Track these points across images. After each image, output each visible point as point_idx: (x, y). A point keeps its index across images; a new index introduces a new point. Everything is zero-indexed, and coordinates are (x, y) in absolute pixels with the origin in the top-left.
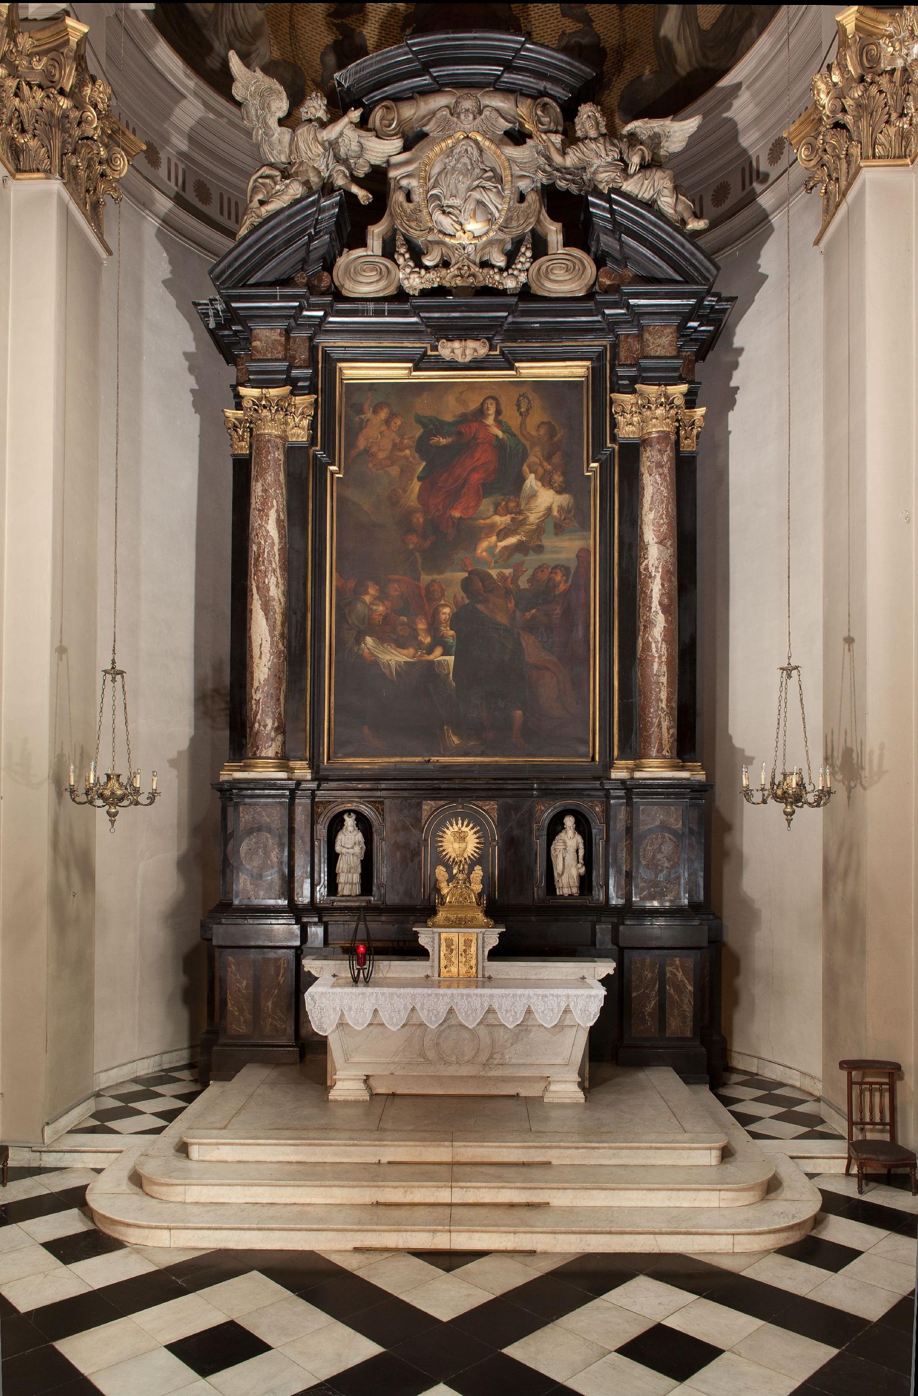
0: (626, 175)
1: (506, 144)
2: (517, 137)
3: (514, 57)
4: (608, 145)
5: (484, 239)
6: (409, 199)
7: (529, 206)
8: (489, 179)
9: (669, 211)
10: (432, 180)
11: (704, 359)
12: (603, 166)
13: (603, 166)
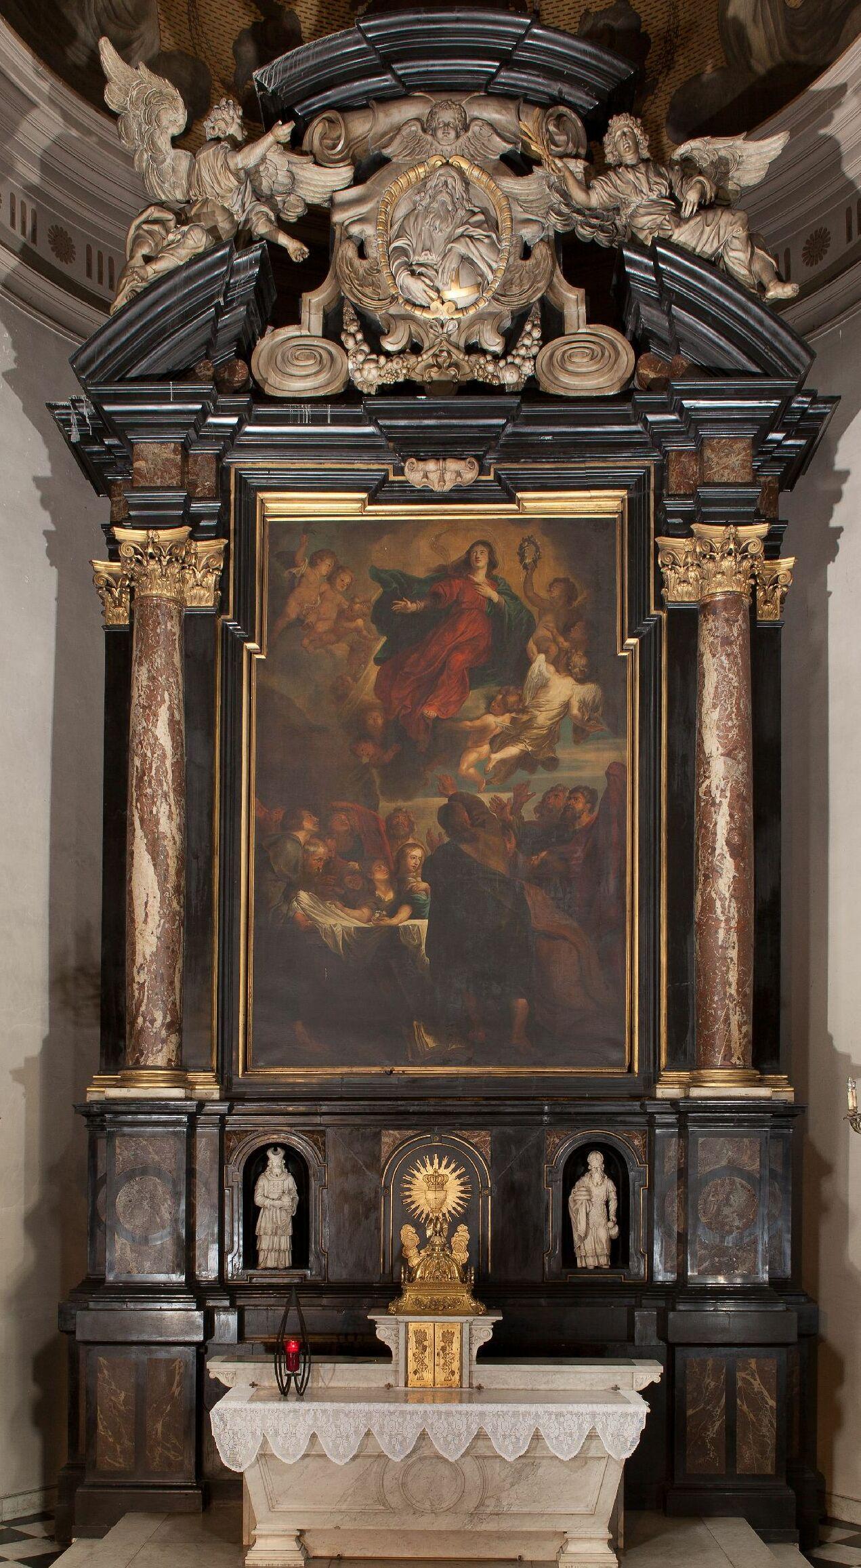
6: (362, 254)
7: (538, 265)
8: (478, 225)
10: (396, 227)
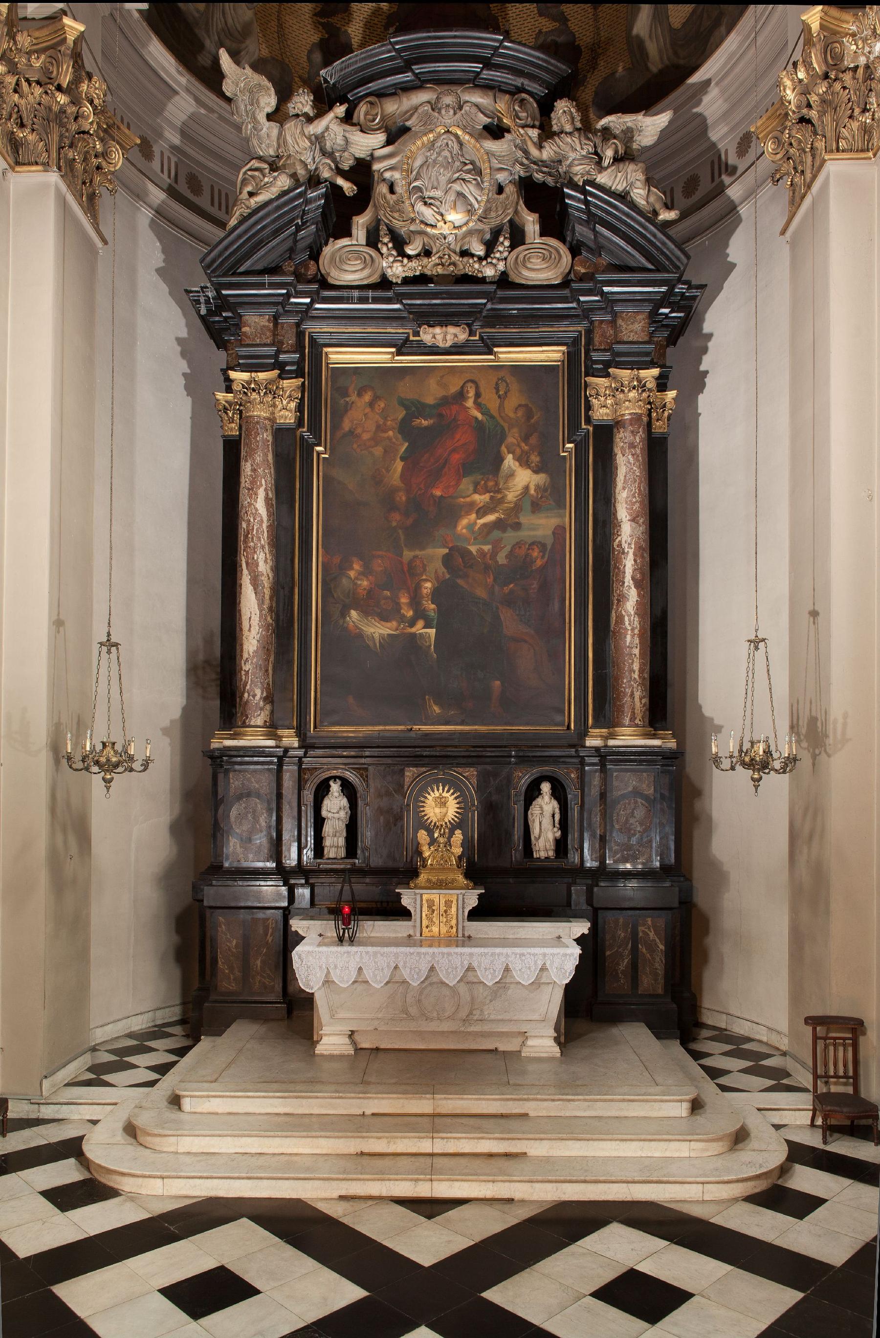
0: (600, 168)
1: (485, 138)
2: (496, 131)
3: (493, 55)
4: (582, 139)
5: (464, 229)
6: (392, 191)
7: (507, 198)
8: (468, 172)
9: (641, 202)
10: (414, 173)
11: (674, 344)
12: (578, 160)
13: (578, 160)
